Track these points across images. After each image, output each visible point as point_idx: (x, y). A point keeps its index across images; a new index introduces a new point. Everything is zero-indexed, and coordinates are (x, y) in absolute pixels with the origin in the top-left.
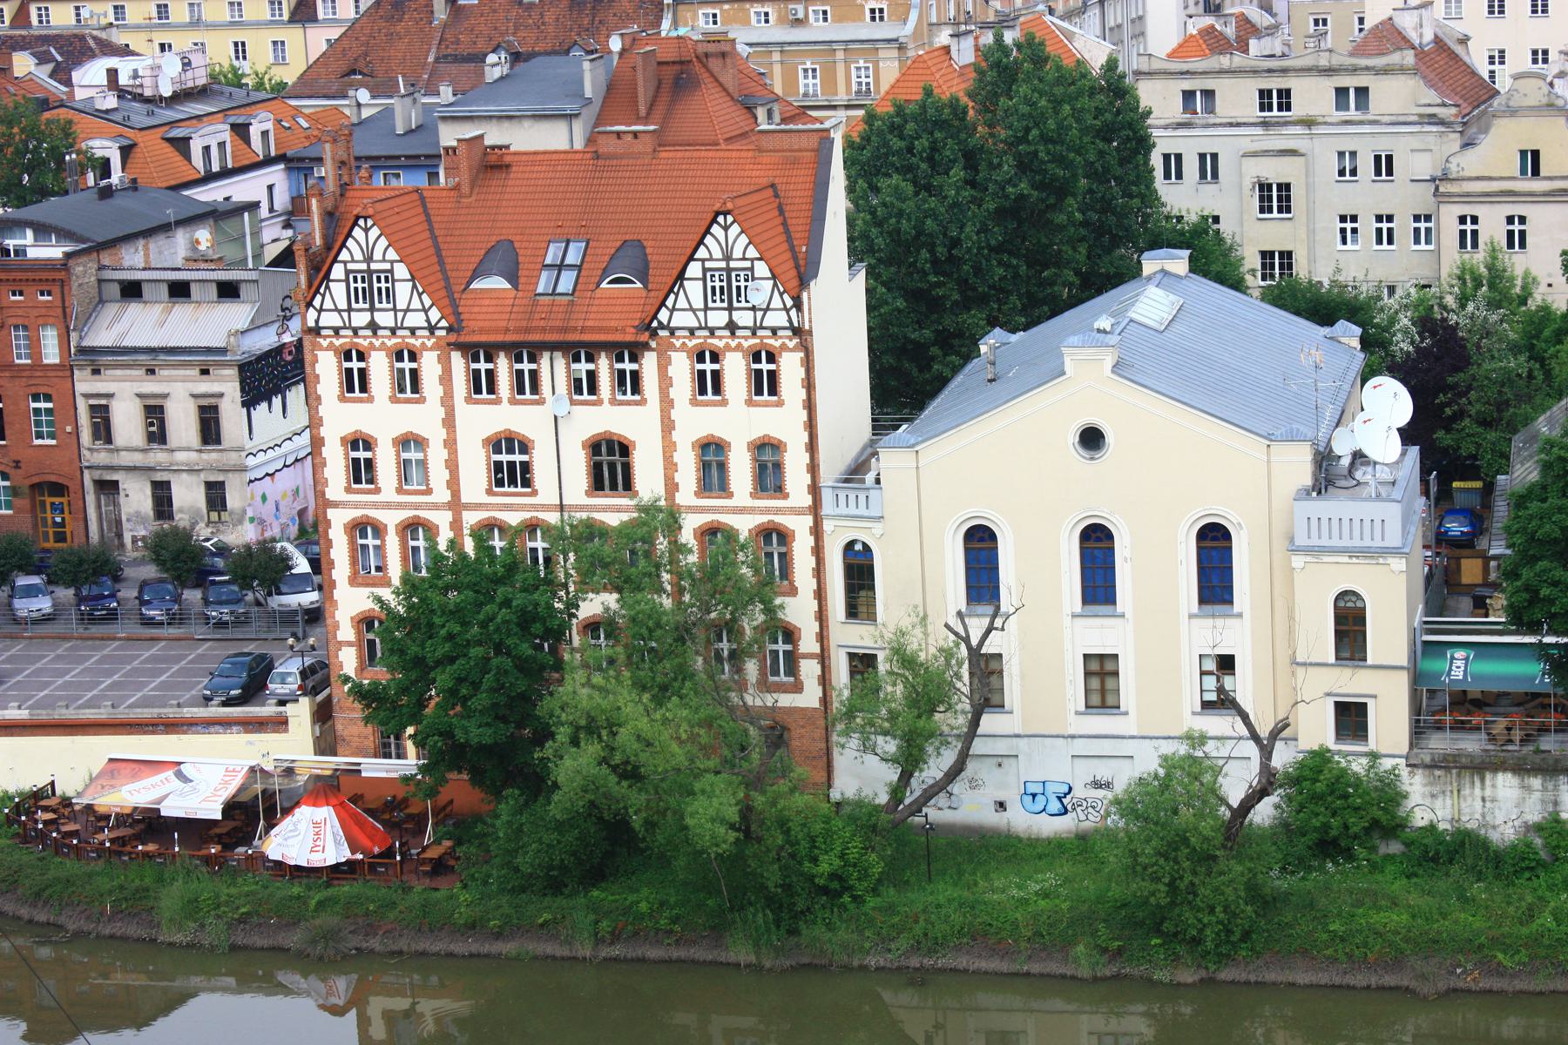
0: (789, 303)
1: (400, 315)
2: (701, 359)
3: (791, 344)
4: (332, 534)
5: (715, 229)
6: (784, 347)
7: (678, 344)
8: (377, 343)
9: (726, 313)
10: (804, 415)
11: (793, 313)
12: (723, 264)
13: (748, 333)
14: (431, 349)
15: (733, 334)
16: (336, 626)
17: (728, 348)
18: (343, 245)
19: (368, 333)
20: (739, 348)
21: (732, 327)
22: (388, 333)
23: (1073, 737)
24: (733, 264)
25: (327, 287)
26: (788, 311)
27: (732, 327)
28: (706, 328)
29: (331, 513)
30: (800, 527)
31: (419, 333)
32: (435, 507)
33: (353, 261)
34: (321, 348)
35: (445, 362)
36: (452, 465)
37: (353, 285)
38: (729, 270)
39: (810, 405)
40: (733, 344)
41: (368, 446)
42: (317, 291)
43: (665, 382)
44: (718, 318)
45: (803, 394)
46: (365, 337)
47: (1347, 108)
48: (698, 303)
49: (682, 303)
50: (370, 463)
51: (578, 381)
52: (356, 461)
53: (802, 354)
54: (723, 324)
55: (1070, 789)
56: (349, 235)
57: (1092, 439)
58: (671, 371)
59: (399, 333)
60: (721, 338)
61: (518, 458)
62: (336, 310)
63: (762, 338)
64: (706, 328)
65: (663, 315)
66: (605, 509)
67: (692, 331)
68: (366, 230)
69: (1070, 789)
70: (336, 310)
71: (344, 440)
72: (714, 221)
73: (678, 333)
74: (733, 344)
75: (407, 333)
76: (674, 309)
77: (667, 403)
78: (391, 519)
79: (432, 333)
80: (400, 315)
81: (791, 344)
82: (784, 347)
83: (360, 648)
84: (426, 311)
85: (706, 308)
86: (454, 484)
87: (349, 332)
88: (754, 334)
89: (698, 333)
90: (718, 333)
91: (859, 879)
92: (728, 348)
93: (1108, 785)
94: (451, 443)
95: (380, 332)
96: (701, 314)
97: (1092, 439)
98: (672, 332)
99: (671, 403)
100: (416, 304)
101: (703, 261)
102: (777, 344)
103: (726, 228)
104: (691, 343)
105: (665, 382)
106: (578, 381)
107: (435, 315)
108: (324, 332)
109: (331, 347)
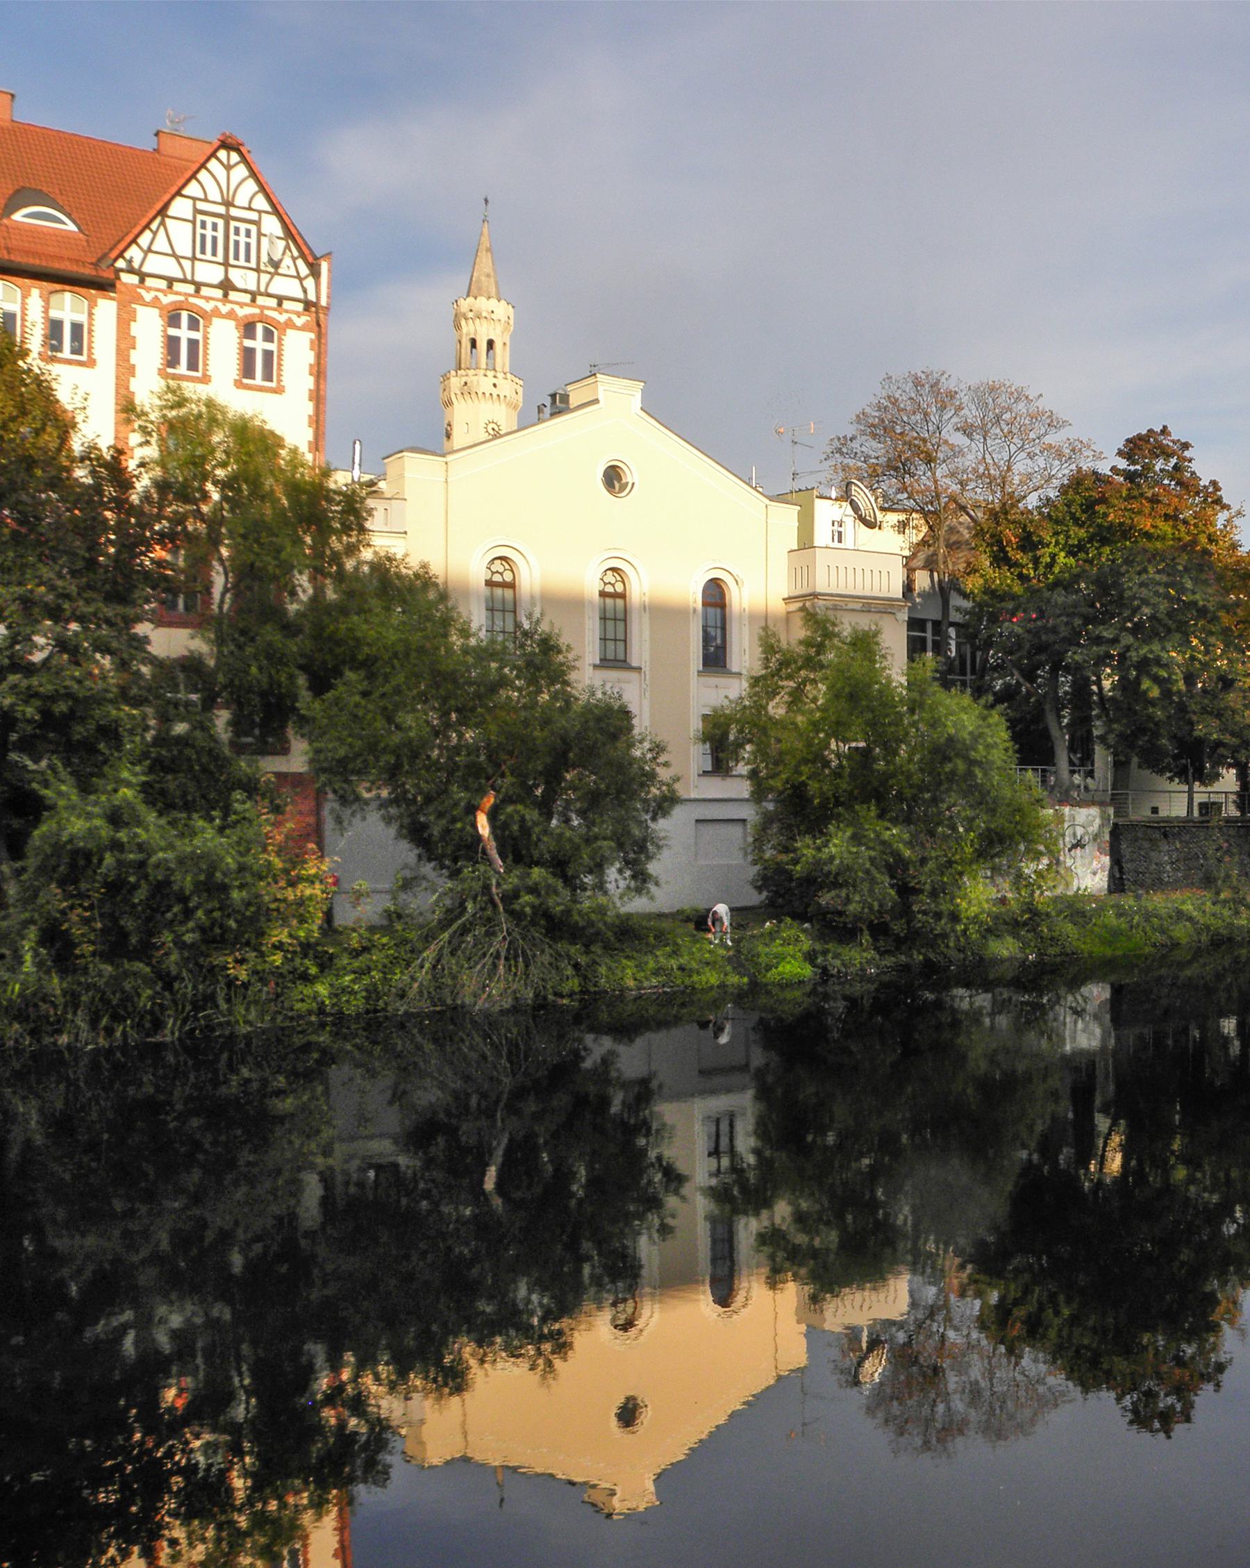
0: (304, 270)
2: (173, 321)
3: (299, 321)
5: (213, 164)
6: (290, 324)
7: (148, 297)
9: (222, 268)
10: (309, 408)
11: (310, 283)
12: (221, 210)
14: (304, 328)
15: (226, 295)
17: (216, 313)
19: (218, 293)
20: (231, 315)
21: (226, 286)
22: (247, 298)
24: (234, 212)
26: (301, 280)
27: (226, 286)
28: (193, 282)
33: (206, 200)
37: (199, 231)
38: (227, 218)
39: (317, 397)
40: (225, 309)
42: (147, 226)
43: (125, 343)
44: (210, 273)
45: (310, 382)
48: (184, 249)
49: (161, 244)
53: (313, 336)
54: (216, 282)
57: (613, 478)
58: (135, 329)
59: (261, 300)
60: (208, 299)
62: (174, 255)
63: (262, 308)
64: (193, 282)
65: (134, 253)
67: (171, 281)
72: (213, 155)
73: (149, 282)
74: (225, 309)
75: (273, 302)
81: (299, 321)
82: (290, 324)
85: (194, 259)
87: (190, 289)
88: (253, 300)
89: (177, 287)
90: (205, 291)
91: (351, 1079)
92: (216, 313)
95: (233, 295)
96: (187, 264)
97: (613, 478)
98: (143, 277)
99: (132, 370)
101: (194, 199)
102: (282, 318)
104: (167, 299)
105: (125, 343)
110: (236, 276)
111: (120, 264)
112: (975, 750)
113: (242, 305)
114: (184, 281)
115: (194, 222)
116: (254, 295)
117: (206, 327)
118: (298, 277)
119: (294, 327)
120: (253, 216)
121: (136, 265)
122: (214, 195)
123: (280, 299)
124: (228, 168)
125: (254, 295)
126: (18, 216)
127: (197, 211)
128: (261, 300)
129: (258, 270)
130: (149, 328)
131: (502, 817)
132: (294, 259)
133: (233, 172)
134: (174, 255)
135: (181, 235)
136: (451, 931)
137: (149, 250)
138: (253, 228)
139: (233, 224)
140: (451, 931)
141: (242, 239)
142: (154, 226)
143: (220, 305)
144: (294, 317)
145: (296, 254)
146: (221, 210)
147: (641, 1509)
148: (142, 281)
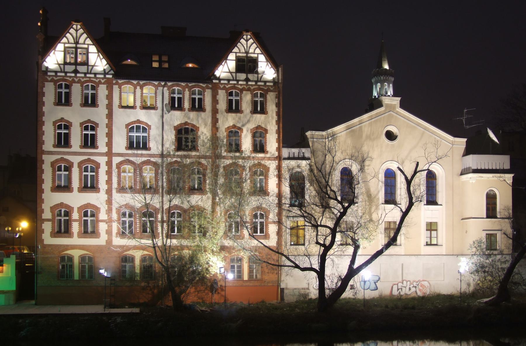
4: (44, 167)
7: (49, 79)
8: (76, 80)
12: (74, 45)
13: (254, 83)
14: (104, 84)
16: (42, 211)
23: (453, 255)
24: (78, 46)
27: (247, 80)
28: (236, 80)
29: (44, 157)
30: (102, 160)
32: (269, 159)
33: (240, 53)
34: (48, 81)
36: (110, 135)
41: (67, 127)
43: (215, 101)
46: (70, 77)
50: (93, 137)
51: (86, 98)
52: (60, 134)
55: (379, 278)
58: (218, 97)
61: (141, 134)
63: (259, 85)
66: (137, 155)
69: (379, 278)
71: (54, 123)
77: (215, 111)
78: (76, 160)
81: (103, 81)
82: (100, 83)
86: (109, 144)
94: (110, 126)
101: (236, 53)
103: (247, 41)
105: (215, 101)
106: (86, 98)
108: (49, 74)
109: (224, 88)
114: (233, 80)
116: (85, 74)
117: (241, 95)
120: (86, 46)
122: (72, 41)
124: (247, 41)
125: (256, 82)
128: (88, 75)
130: (222, 96)
132: (101, 59)
133: (78, 32)
136: (87, 270)
139: (79, 50)
140: (87, 270)
143: (75, 79)
144: (81, 79)
146: (74, 45)
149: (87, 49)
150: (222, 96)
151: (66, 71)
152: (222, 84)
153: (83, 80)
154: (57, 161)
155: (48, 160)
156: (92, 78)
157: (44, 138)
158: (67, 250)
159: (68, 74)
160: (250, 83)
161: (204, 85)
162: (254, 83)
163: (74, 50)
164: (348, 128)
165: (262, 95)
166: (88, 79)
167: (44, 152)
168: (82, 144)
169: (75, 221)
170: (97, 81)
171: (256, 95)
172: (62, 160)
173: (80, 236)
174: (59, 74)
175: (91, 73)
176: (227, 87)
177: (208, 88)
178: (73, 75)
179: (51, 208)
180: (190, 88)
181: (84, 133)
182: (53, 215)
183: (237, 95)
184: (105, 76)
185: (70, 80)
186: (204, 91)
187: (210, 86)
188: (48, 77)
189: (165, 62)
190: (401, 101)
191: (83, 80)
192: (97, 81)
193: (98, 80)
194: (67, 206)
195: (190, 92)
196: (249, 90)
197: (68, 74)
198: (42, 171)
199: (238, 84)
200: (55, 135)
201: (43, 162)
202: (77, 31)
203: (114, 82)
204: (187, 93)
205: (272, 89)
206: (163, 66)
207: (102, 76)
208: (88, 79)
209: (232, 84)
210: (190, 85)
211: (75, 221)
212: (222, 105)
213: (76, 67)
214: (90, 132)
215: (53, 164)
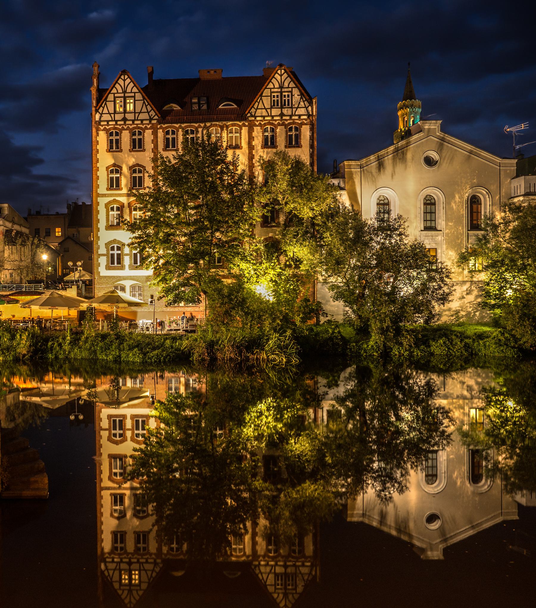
1: (137, 115)
7: (257, 123)
8: (125, 127)
12: (122, 95)
13: (288, 118)
14: (149, 129)
18: (114, 86)
21: (282, 115)
22: (131, 122)
25: (106, 104)
27: (282, 115)
28: (114, 120)
29: (99, 199)
31: (144, 122)
33: (118, 93)
35: (155, 134)
37: (273, 99)
42: (101, 106)
43: (251, 138)
46: (120, 125)
47: (116, 430)
48: (267, 106)
49: (105, 111)
56: (117, 82)
58: (254, 134)
62: (265, 108)
63: (137, 124)
64: (271, 116)
68: (124, 80)
70: (109, 113)
74: (125, 127)
75: (139, 122)
76: (257, 108)
79: (150, 122)
80: (137, 115)
81: (149, 127)
82: (146, 128)
83: (108, 258)
84: (148, 112)
88: (291, 119)
92: (123, 129)
93: (430, 203)
95: (127, 122)
96: (113, 115)
100: (144, 110)
107: (152, 113)
108: (102, 123)
110: (285, 111)
111: (249, 115)
112: (344, 479)
113: (131, 125)
114: (112, 121)
115: (271, 96)
116: (291, 116)
118: (305, 107)
119: (148, 129)
121: (253, 114)
123: (142, 121)
124: (124, 80)
125: (133, 121)
126: (220, 107)
127: (271, 92)
128: (136, 122)
129: (292, 108)
130: (257, 132)
131: (480, 293)
134: (265, 108)
135: (267, 102)
137: (257, 108)
138: (290, 94)
139: (284, 94)
141: (287, 99)
142: (103, 106)
143: (124, 126)
145: (147, 104)
147: (305, 538)
148: (255, 118)
149: (291, 92)
150: (257, 132)
151: (272, 115)
152: (257, 121)
153: (131, 127)
154: (110, 202)
155: (103, 201)
156: (296, 119)
157: (99, 182)
158: (119, 280)
159: (275, 118)
160: (284, 118)
161: (240, 124)
162: (288, 118)
163: (122, 99)
164: (471, 152)
165: (140, 133)
166: (135, 126)
167: (98, 195)
168: (108, 186)
169: (127, 255)
170: (143, 127)
171: (266, 130)
172: (115, 201)
173: (131, 268)
174: (266, 118)
175: (137, 120)
176: (263, 123)
177: (244, 125)
178: (122, 123)
179: (106, 244)
180: (163, 129)
181: (110, 176)
182: (108, 251)
183: (140, 133)
184: (150, 122)
185: (120, 127)
186: (241, 129)
187: (247, 124)
188: (100, 127)
189: (195, 103)
190: (441, 125)
191: (131, 127)
192: (143, 127)
193: (145, 125)
194: (119, 242)
195: (227, 131)
196: (283, 124)
197: (275, 118)
198: (98, 212)
199: (116, 124)
200: (108, 179)
201: (98, 204)
202: (281, 75)
203: (159, 126)
204: (180, 132)
205: (305, 122)
206: (203, 108)
207: (148, 122)
208: (135, 126)
209: (267, 120)
210: (164, 126)
211: (127, 255)
212: (258, 142)
213: (125, 115)
214: (137, 175)
215: (106, 205)
